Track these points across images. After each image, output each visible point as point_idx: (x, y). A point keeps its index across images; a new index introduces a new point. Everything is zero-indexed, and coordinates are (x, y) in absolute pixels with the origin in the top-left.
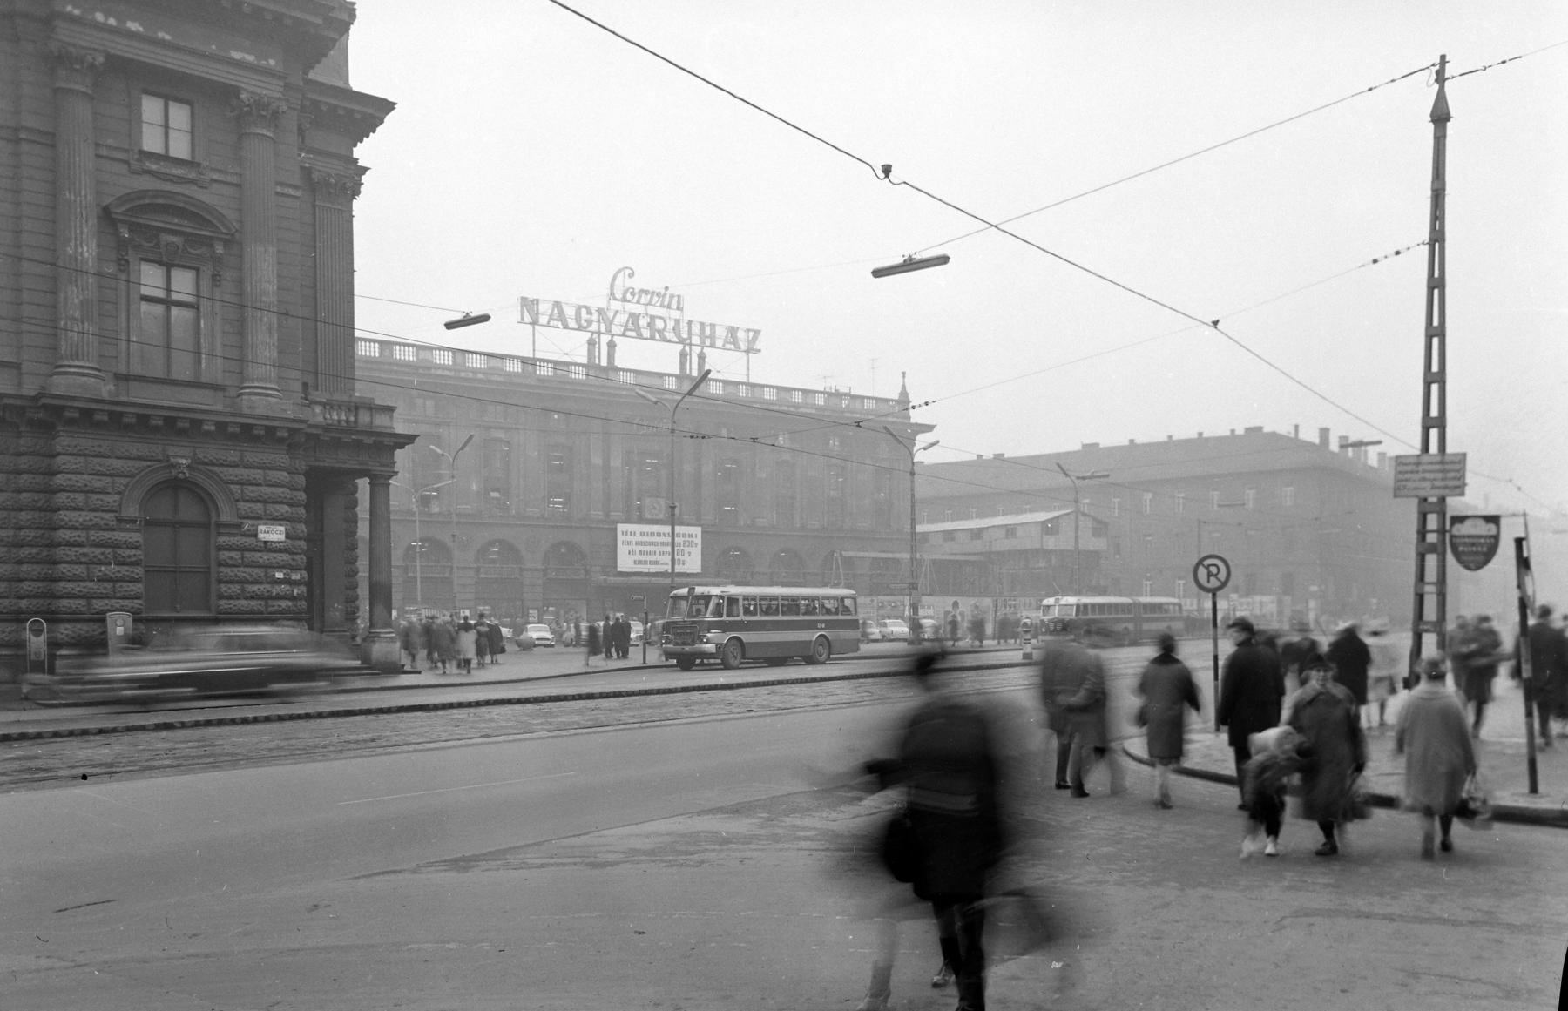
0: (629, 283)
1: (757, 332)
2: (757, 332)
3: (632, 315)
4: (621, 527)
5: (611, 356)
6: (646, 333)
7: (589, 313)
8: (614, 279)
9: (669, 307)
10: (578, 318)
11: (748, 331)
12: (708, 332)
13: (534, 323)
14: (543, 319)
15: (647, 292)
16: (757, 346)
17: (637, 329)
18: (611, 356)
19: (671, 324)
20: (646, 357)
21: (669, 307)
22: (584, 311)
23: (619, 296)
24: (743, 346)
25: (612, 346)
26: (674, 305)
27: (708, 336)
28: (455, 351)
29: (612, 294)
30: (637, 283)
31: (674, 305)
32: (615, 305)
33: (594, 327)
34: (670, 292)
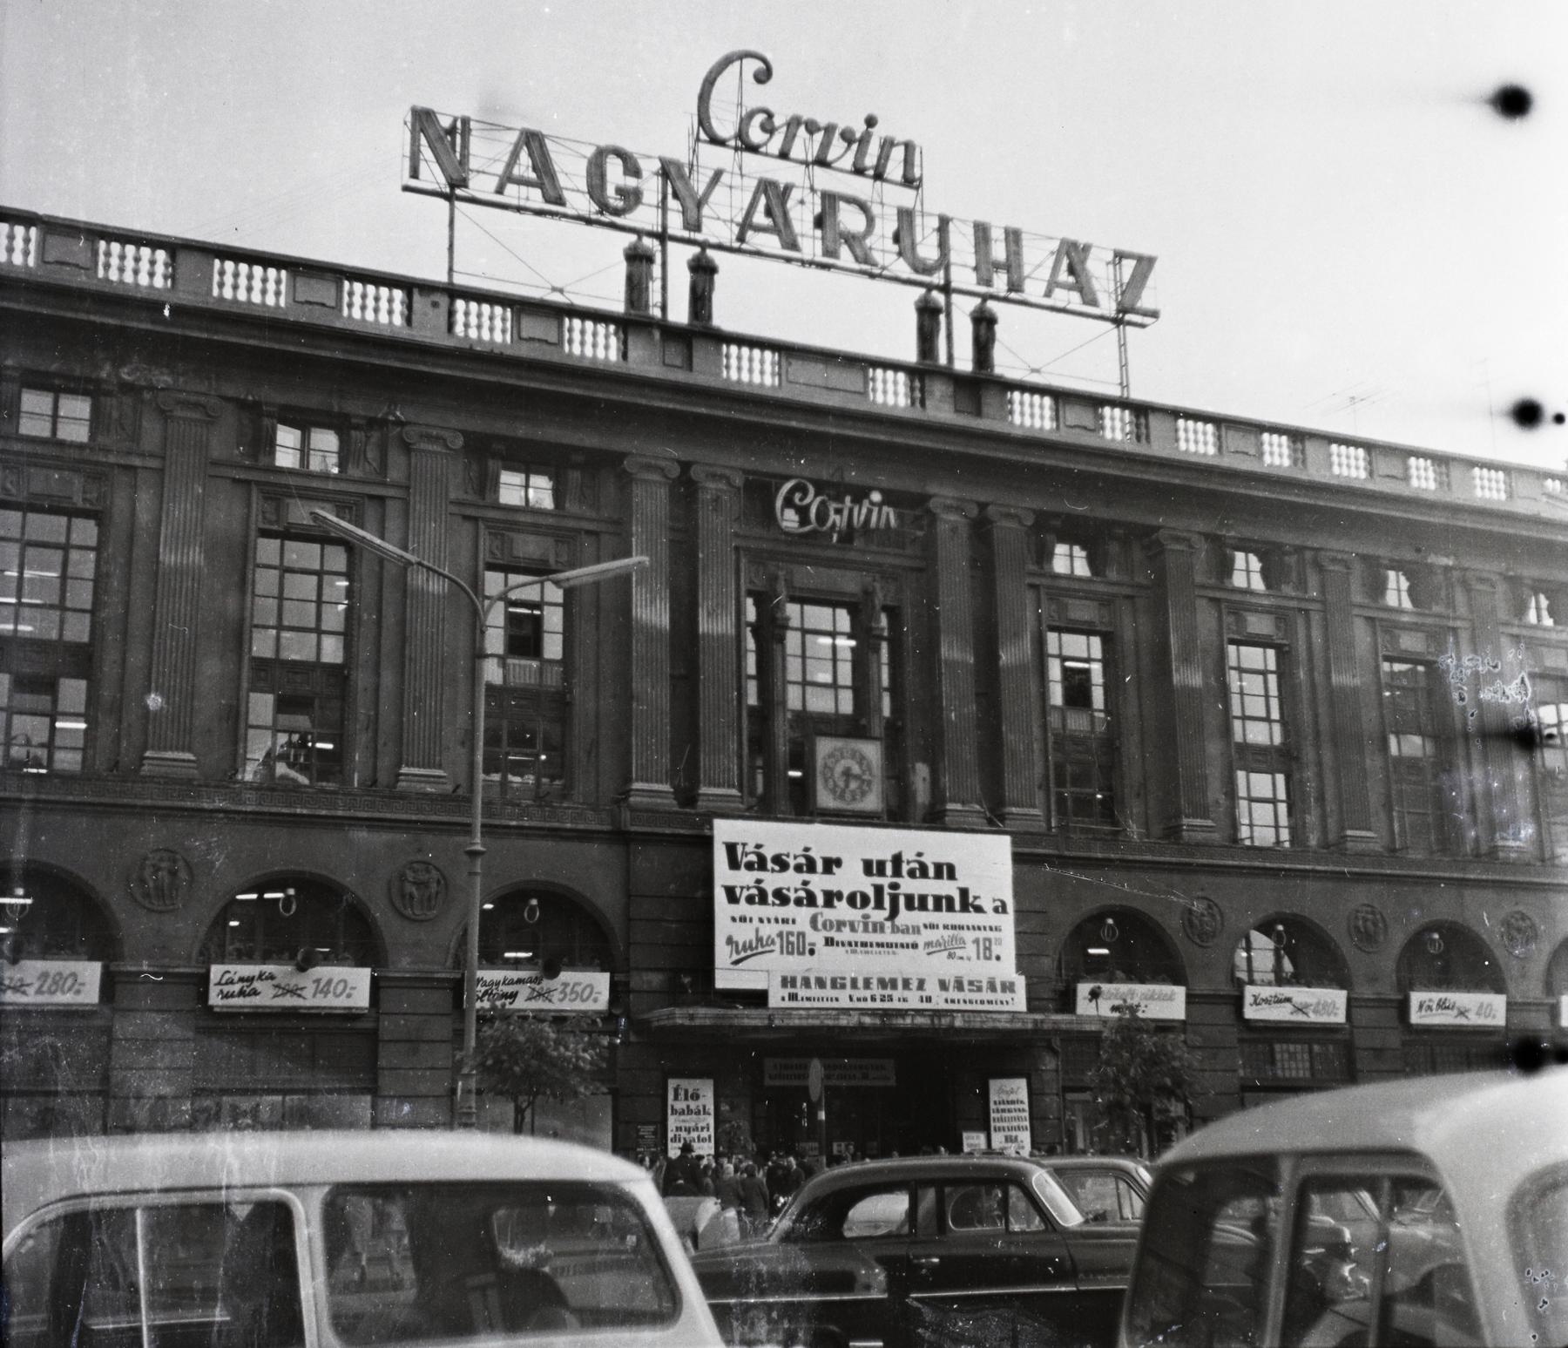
0: (758, 96)
1: (1145, 264)
2: (1145, 264)
3: (765, 186)
4: (725, 830)
5: (700, 300)
6: (811, 246)
7: (632, 169)
8: (709, 83)
9: (879, 176)
10: (596, 186)
11: (1120, 256)
12: (999, 252)
13: (454, 190)
14: (481, 185)
15: (812, 128)
16: (1146, 301)
17: (782, 227)
18: (700, 300)
19: (887, 224)
20: (799, 309)
21: (879, 176)
22: (614, 168)
23: (725, 126)
24: (1108, 306)
25: (703, 270)
26: (895, 170)
27: (1002, 259)
28: (176, 248)
29: (703, 120)
30: (781, 99)
31: (895, 170)
32: (712, 157)
33: (645, 217)
34: (878, 133)
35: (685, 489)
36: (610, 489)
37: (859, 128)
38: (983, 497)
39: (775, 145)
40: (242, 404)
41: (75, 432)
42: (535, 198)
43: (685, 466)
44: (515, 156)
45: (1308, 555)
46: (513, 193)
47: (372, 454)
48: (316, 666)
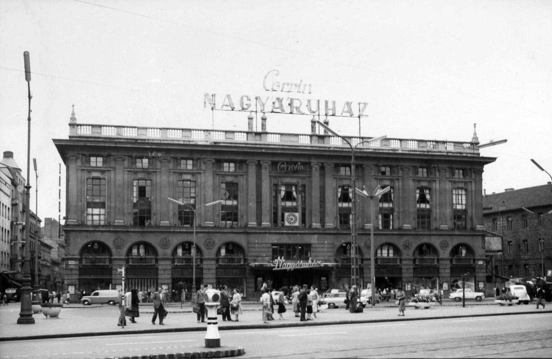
2: (365, 104)
5: (263, 126)
15: (288, 84)
18: (263, 126)
19: (305, 103)
22: (245, 99)
26: (307, 91)
31: (307, 91)
35: (322, 168)
36: (244, 166)
37: (299, 83)
38: (322, 161)
39: (280, 89)
40: (129, 156)
41: (100, 164)
42: (348, 115)
43: (259, 161)
44: (225, 100)
45: (400, 167)
46: (344, 114)
47: (198, 164)
48: (462, 210)
